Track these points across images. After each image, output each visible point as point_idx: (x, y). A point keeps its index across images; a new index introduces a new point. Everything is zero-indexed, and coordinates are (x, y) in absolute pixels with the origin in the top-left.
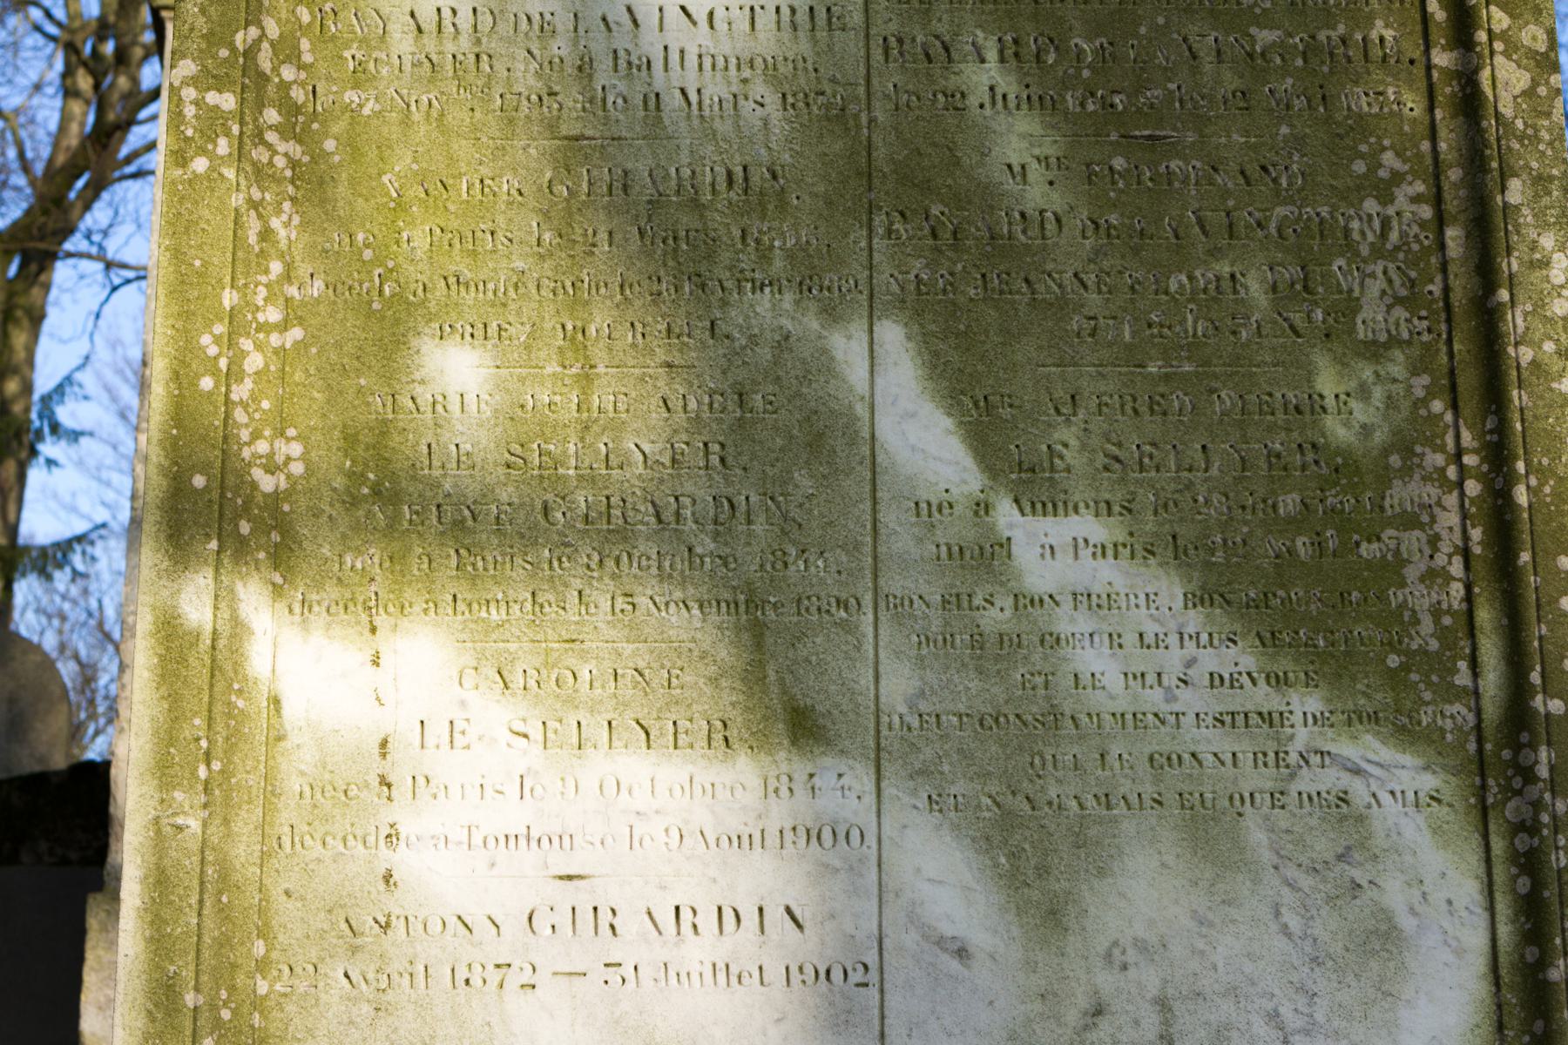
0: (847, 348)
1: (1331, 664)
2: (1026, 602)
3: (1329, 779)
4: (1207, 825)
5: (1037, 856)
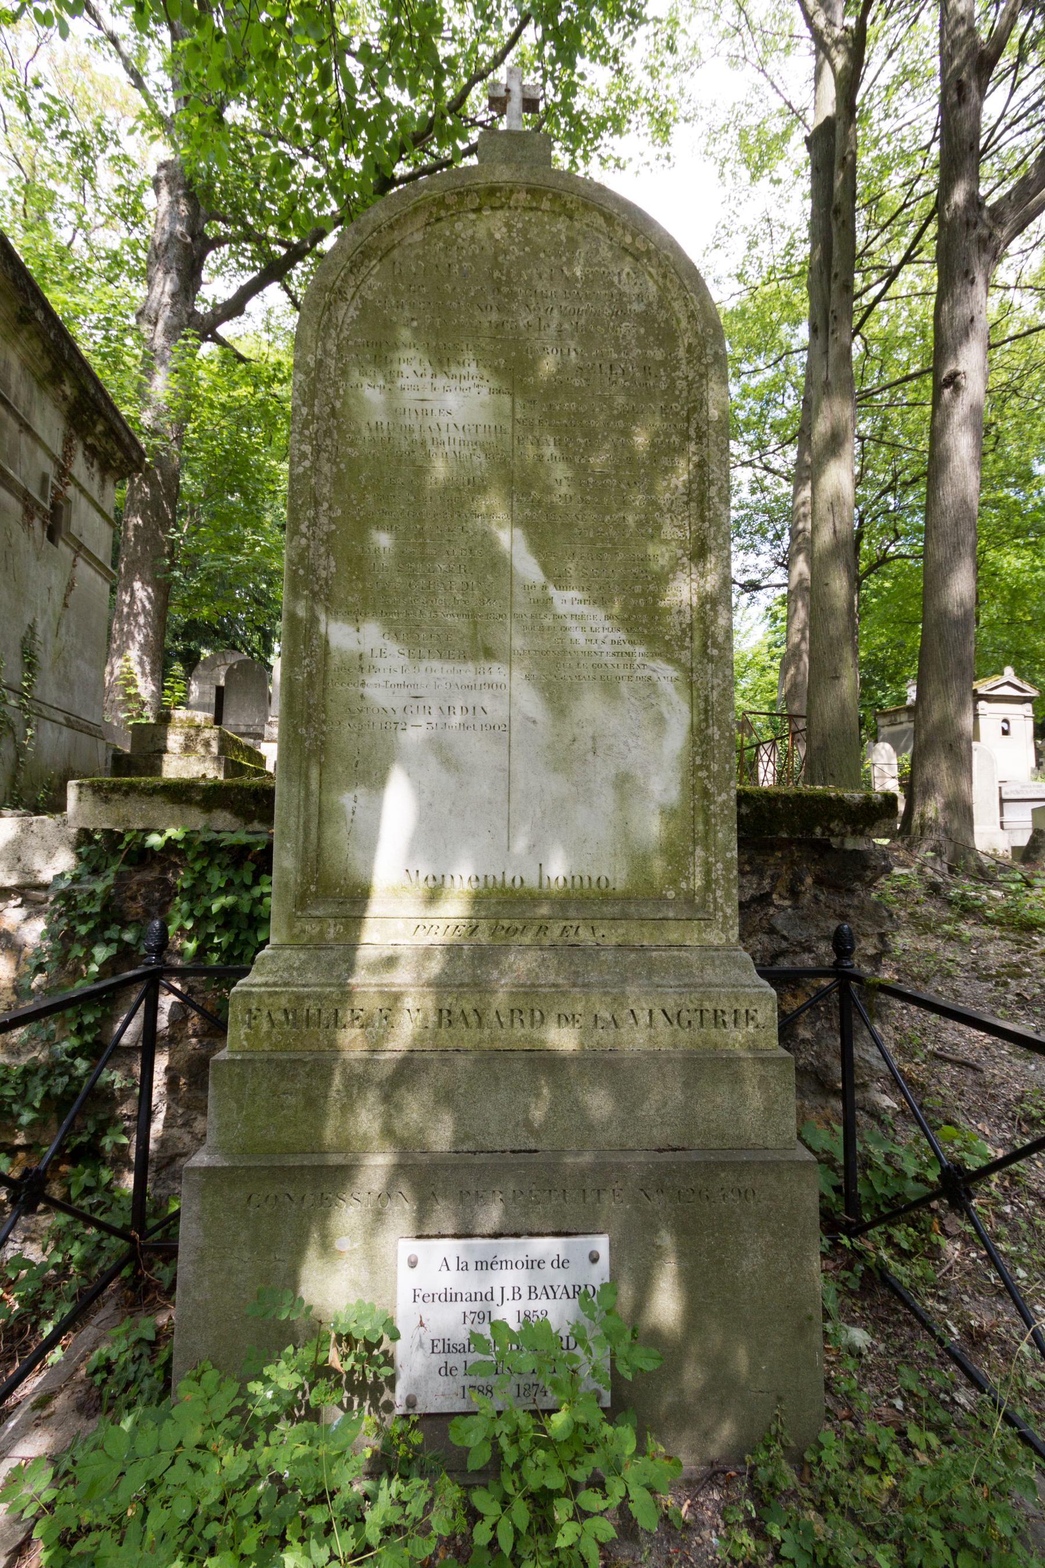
2: (556, 617)
3: (647, 672)
4: (609, 686)
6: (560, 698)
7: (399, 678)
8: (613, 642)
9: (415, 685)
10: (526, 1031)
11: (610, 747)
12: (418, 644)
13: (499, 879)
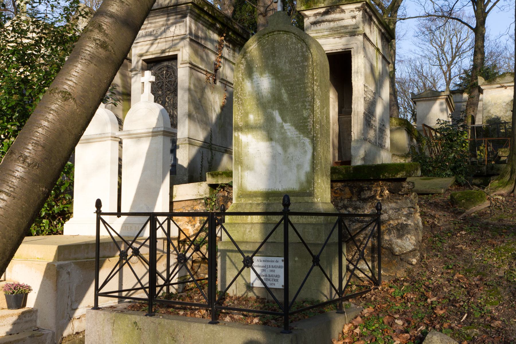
0: (274, 113)
1: (303, 133)
2: (285, 130)
3: (303, 141)
4: (295, 145)
5: (285, 147)
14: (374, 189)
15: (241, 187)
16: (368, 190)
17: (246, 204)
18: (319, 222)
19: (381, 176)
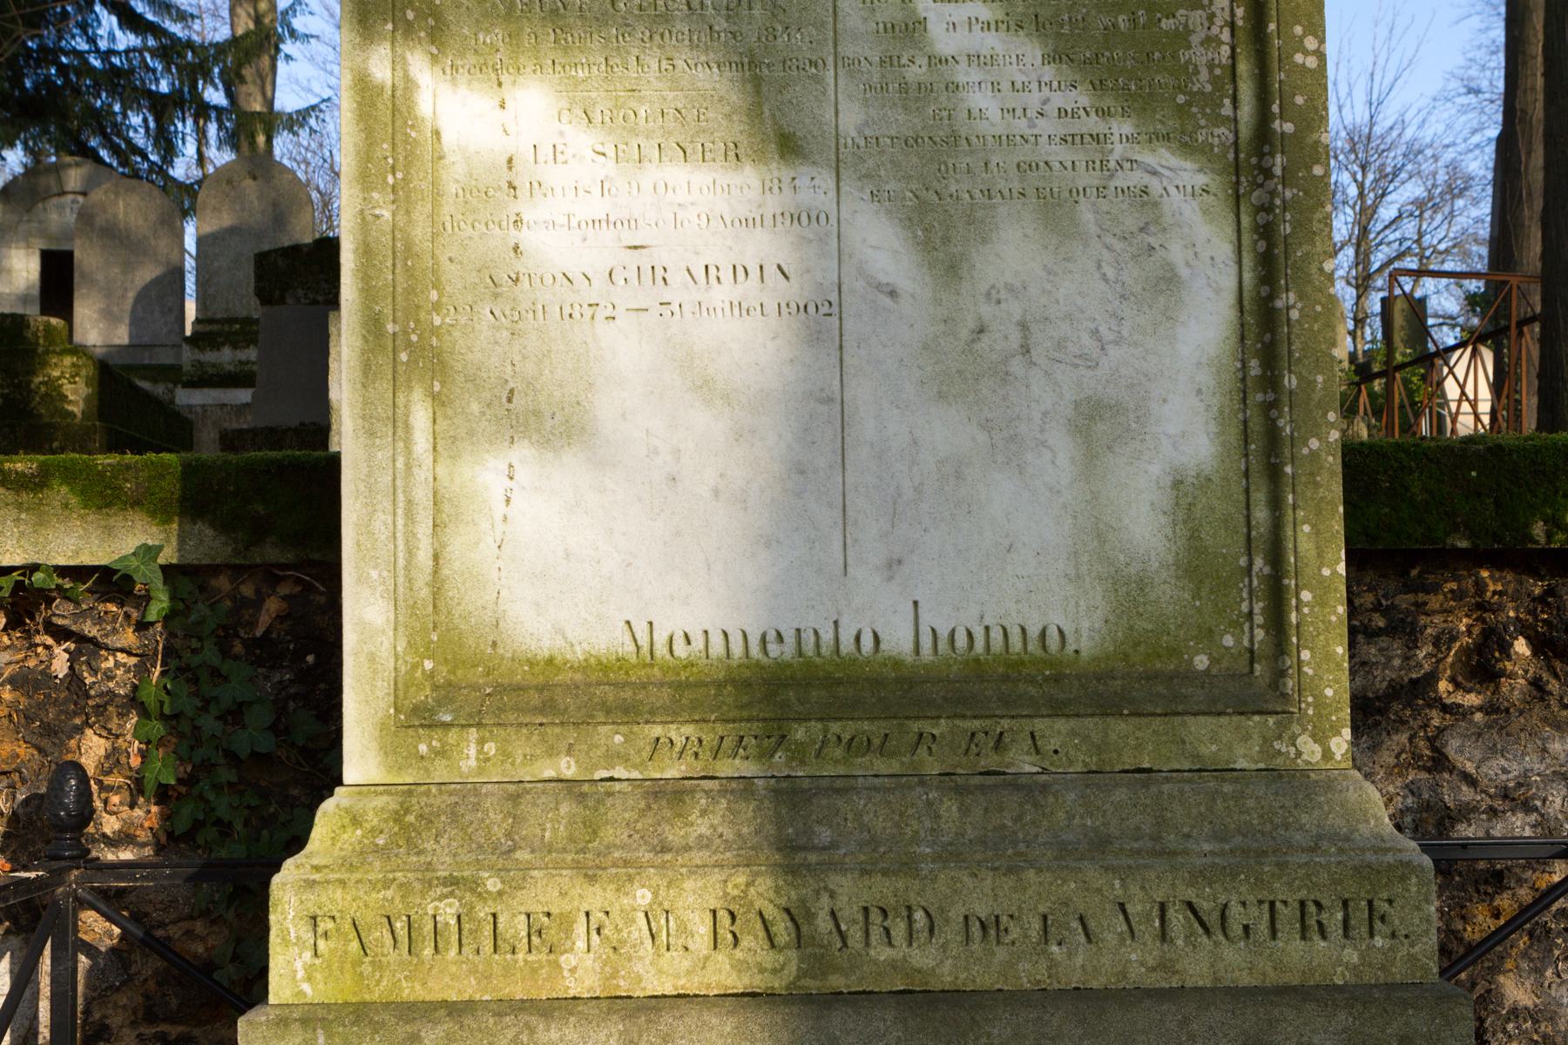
1: (1139, 102)
2: (935, 61)
3: (1136, 178)
4: (1054, 209)
6: (946, 240)
7: (596, 207)
8: (1063, 113)
9: (631, 223)
10: (901, 950)
11: (1060, 345)
12: (634, 131)
13: (827, 636)
14: (1433, 625)
15: (430, 613)
16: (1391, 631)
17: (516, 793)
18: (1399, 973)
19: (1538, 530)
